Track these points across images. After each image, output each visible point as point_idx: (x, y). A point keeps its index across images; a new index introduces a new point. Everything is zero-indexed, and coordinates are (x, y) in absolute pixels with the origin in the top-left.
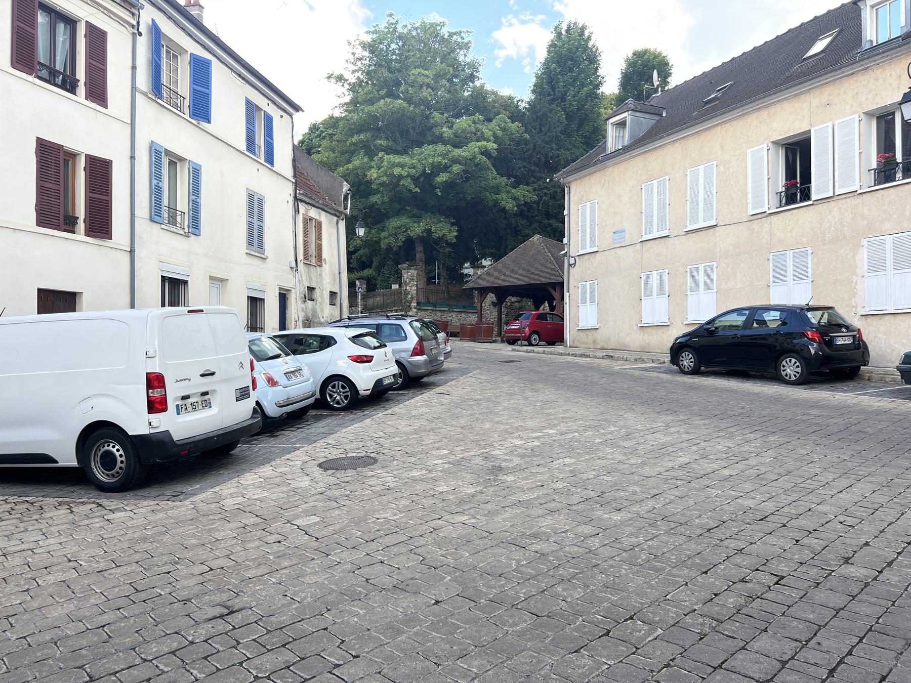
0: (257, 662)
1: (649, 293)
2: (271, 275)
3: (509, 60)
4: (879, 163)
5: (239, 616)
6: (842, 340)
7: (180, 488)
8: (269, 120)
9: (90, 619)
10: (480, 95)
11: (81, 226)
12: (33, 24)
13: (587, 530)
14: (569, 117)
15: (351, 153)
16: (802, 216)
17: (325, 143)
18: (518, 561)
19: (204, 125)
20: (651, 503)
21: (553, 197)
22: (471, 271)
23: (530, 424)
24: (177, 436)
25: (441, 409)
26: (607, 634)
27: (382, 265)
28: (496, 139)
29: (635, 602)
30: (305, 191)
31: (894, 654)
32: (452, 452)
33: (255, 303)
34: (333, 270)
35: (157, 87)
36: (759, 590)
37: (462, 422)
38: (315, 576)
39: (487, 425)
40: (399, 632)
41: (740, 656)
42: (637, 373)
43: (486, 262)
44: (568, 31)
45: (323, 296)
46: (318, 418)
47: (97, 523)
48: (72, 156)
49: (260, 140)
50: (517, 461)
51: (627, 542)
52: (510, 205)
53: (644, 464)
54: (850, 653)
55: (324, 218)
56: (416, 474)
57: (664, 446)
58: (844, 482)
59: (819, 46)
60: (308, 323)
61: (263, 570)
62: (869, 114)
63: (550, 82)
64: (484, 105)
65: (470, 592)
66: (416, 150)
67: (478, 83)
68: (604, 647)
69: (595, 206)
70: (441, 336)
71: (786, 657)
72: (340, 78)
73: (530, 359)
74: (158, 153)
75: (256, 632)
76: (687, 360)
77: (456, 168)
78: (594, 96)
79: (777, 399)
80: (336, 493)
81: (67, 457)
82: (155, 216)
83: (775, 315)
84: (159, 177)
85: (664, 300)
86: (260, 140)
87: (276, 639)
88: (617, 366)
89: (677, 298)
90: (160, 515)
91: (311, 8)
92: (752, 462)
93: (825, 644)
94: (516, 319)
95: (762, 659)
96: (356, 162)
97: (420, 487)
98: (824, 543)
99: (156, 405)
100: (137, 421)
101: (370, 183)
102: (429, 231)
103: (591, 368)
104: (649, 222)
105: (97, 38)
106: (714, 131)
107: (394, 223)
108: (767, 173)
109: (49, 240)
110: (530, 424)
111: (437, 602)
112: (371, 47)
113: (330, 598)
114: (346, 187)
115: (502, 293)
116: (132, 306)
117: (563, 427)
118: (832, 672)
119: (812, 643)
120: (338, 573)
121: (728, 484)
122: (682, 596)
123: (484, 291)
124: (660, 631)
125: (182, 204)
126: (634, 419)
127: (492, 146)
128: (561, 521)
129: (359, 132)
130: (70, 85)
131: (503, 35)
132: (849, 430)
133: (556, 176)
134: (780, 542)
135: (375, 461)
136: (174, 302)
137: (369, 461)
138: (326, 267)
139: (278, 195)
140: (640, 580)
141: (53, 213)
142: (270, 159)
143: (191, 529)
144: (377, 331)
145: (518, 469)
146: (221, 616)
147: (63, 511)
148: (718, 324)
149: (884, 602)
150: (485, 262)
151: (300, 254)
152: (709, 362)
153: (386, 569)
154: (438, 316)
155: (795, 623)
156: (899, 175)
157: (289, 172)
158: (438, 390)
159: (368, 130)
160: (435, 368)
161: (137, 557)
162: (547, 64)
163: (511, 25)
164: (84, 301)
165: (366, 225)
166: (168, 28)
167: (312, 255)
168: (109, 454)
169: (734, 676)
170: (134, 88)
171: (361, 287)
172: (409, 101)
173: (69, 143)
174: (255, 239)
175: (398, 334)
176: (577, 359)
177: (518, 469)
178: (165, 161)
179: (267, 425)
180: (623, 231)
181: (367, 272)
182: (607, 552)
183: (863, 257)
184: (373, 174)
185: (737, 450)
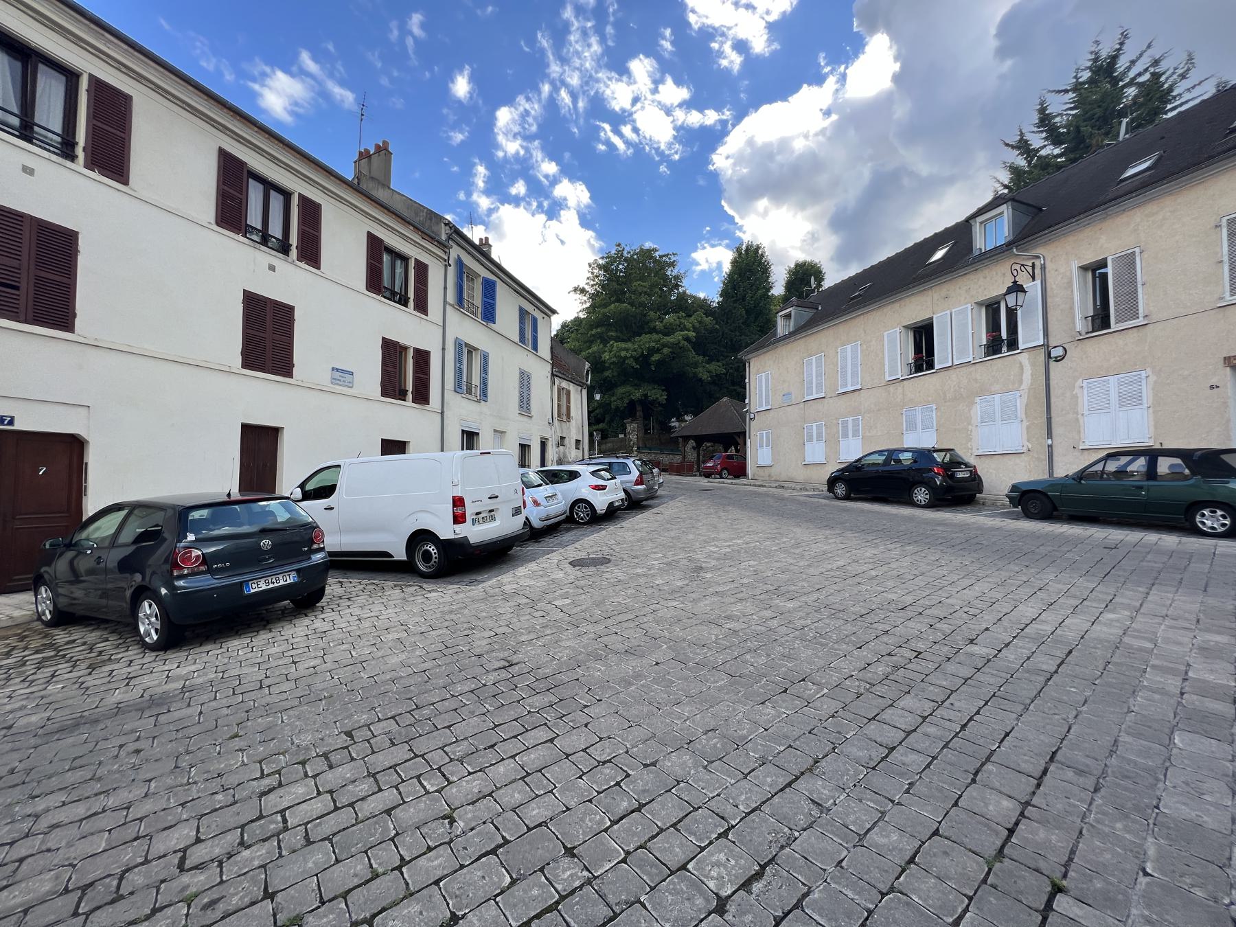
0: (530, 700)
1: (810, 440)
2: (535, 429)
3: (703, 272)
4: (988, 340)
5: (516, 667)
6: (961, 474)
7: (474, 577)
8: (535, 321)
9: (416, 665)
10: (683, 297)
11: (410, 396)
12: (380, 261)
13: (768, 614)
14: (747, 311)
15: (590, 342)
16: (927, 382)
17: (573, 335)
18: (716, 636)
19: (491, 325)
20: (816, 595)
21: (737, 370)
22: (677, 424)
23: (722, 536)
24: (473, 540)
25: (656, 524)
26: (785, 691)
27: (612, 421)
28: (695, 329)
29: (807, 668)
30: (559, 369)
31: (1015, 716)
32: (665, 556)
33: (524, 448)
34: (578, 425)
35: (460, 300)
36: (903, 662)
37: (672, 534)
38: (569, 643)
39: (691, 537)
40: (630, 684)
41: (889, 711)
42: (802, 499)
43: (688, 418)
44: (747, 250)
45: (571, 443)
46: (568, 530)
47: (420, 599)
48: (404, 349)
49: (529, 335)
50: (714, 563)
51: (799, 623)
52: (705, 376)
53: (809, 565)
54: (978, 713)
55: (572, 388)
56: (640, 571)
57: (825, 553)
58: (967, 582)
59: (939, 254)
60: (560, 462)
61: (532, 636)
62: (979, 304)
63: (734, 288)
64: (687, 306)
65: (681, 657)
66: (637, 339)
67: (681, 290)
68: (784, 701)
69: (770, 378)
70: (656, 470)
71: (926, 714)
72: (583, 291)
73: (721, 489)
74: (460, 345)
75: (528, 679)
76: (840, 489)
77: (666, 351)
78: (766, 297)
79: (911, 519)
80: (582, 583)
81: (400, 554)
82: (458, 388)
83: (908, 455)
84: (461, 362)
85: (822, 444)
86: (529, 335)
87: (542, 686)
88: (787, 494)
89: (832, 443)
90: (462, 595)
91: (563, 242)
92: (894, 565)
93: (957, 704)
94: (711, 458)
95: (906, 714)
96: (594, 348)
97: (642, 581)
98: (953, 628)
99: (459, 519)
100: (446, 530)
101: (604, 362)
102: (646, 396)
103: (767, 495)
104: (810, 388)
105: (422, 269)
106: (857, 320)
107: (621, 390)
108: (900, 349)
109: (389, 406)
110: (722, 536)
111: (657, 664)
112: (604, 268)
113: (580, 657)
114: (587, 365)
115: (700, 440)
116: (442, 450)
117: (747, 538)
118: (963, 727)
119: (947, 704)
120: (585, 640)
121: (876, 582)
122: (843, 665)
123: (686, 439)
124: (826, 691)
125: (476, 380)
126: (801, 532)
127: (692, 334)
128: (748, 607)
129: (597, 327)
130: (404, 302)
131: (698, 256)
132: (970, 543)
133: (740, 355)
134: (916, 626)
135: (609, 561)
136: (470, 447)
137: (605, 561)
138: (573, 422)
139: (541, 371)
140: (810, 652)
141: (392, 387)
142: (535, 347)
143: (482, 606)
144: (609, 468)
145: (712, 569)
146: (504, 668)
147: (397, 591)
148: (863, 462)
149: (1004, 675)
150: (687, 418)
151: (554, 413)
152: (857, 491)
153: (620, 639)
154: (653, 457)
155: (932, 688)
156: (1004, 349)
157: (548, 356)
158: (654, 510)
159: (603, 325)
160: (651, 495)
161: (446, 624)
162: (731, 275)
163: (704, 248)
164: (411, 447)
165: (601, 392)
166: (468, 261)
167: (564, 414)
168: (427, 551)
169: (885, 726)
170: (445, 302)
171: (597, 438)
172: (632, 305)
173: (403, 341)
174: (525, 405)
175: (624, 470)
176: (756, 489)
177: (712, 569)
178: (465, 351)
179: (534, 534)
180: (789, 394)
181: (601, 426)
182: (783, 630)
183: (977, 411)
184: (606, 356)
185: (881, 556)
